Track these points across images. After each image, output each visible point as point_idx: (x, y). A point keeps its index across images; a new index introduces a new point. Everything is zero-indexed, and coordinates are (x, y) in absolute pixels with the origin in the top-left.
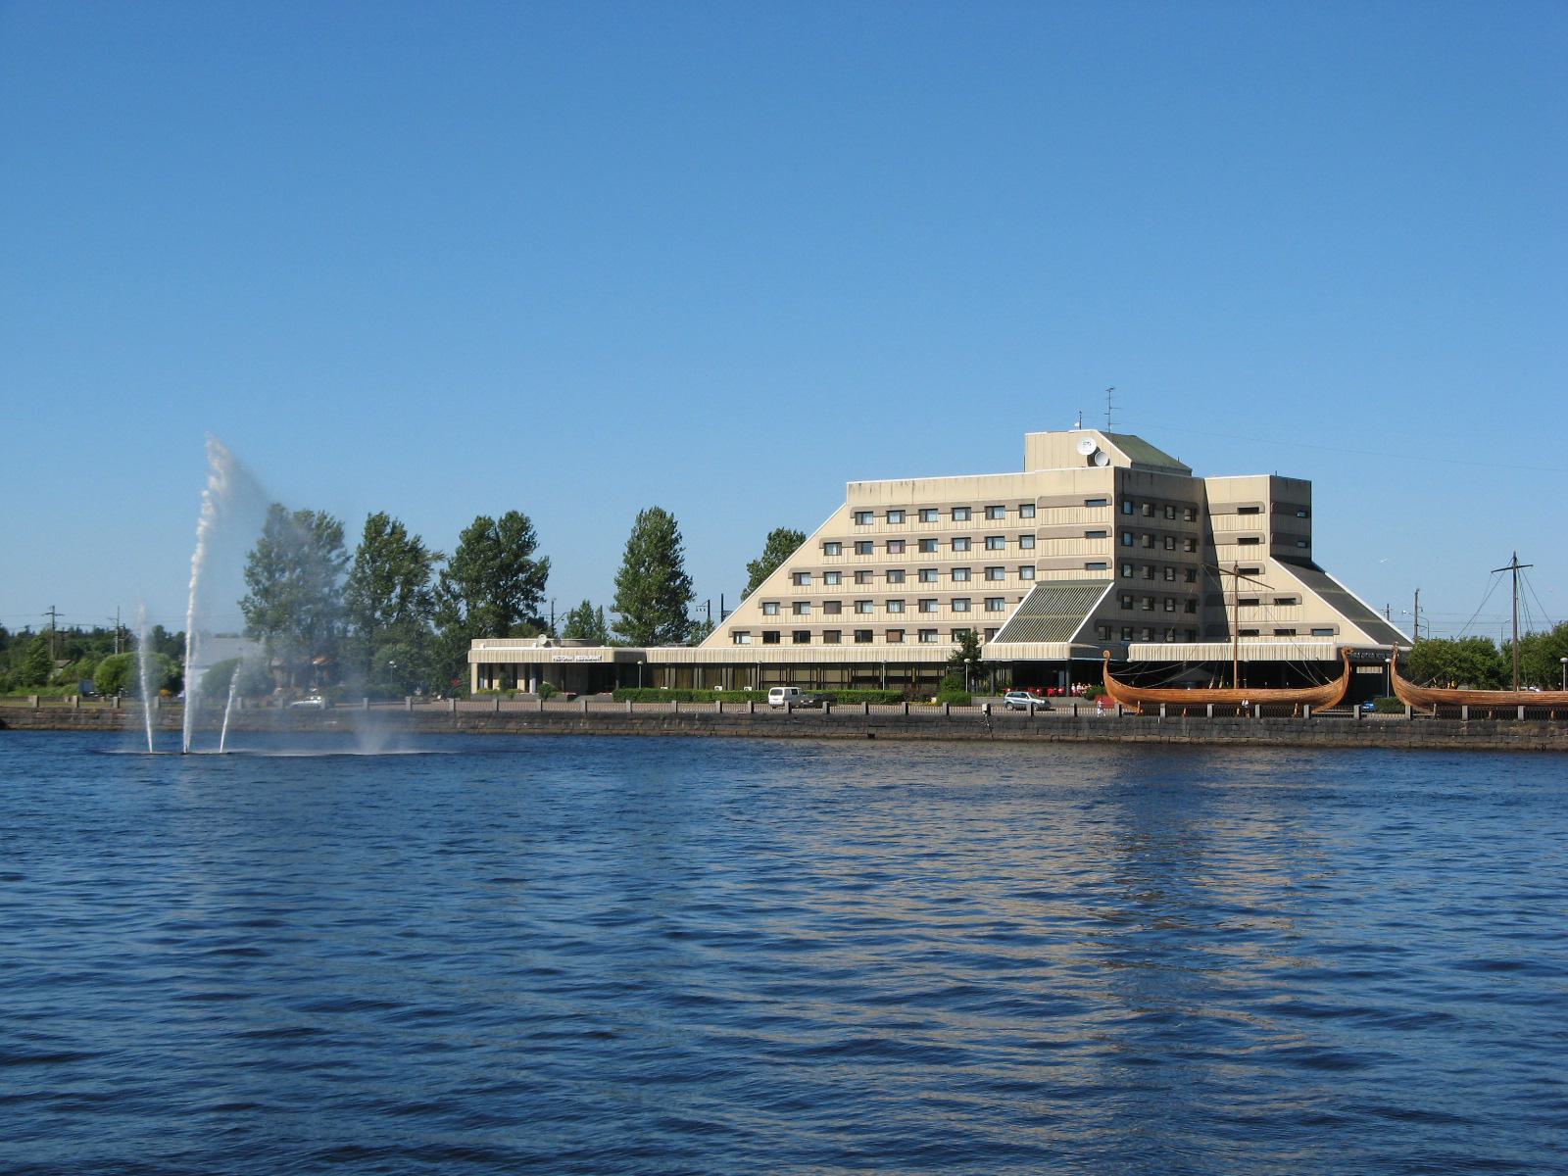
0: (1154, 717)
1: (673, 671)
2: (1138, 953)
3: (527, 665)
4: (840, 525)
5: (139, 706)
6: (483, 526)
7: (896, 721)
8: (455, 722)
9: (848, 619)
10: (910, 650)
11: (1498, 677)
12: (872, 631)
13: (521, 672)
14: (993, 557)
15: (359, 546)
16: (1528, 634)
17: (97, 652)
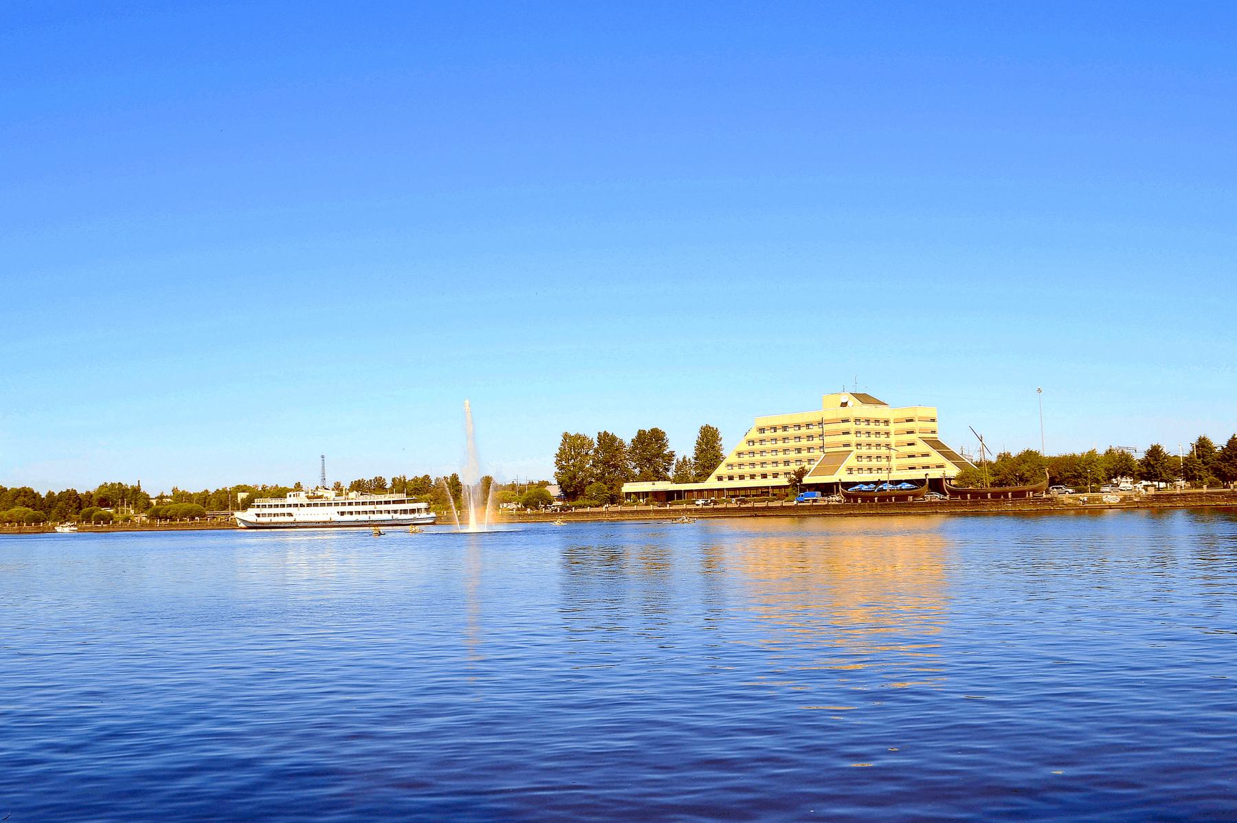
3: (643, 492)
4: (755, 435)
7: (763, 509)
9: (758, 470)
10: (770, 482)
13: (641, 496)
14: (786, 445)
16: (394, 480)
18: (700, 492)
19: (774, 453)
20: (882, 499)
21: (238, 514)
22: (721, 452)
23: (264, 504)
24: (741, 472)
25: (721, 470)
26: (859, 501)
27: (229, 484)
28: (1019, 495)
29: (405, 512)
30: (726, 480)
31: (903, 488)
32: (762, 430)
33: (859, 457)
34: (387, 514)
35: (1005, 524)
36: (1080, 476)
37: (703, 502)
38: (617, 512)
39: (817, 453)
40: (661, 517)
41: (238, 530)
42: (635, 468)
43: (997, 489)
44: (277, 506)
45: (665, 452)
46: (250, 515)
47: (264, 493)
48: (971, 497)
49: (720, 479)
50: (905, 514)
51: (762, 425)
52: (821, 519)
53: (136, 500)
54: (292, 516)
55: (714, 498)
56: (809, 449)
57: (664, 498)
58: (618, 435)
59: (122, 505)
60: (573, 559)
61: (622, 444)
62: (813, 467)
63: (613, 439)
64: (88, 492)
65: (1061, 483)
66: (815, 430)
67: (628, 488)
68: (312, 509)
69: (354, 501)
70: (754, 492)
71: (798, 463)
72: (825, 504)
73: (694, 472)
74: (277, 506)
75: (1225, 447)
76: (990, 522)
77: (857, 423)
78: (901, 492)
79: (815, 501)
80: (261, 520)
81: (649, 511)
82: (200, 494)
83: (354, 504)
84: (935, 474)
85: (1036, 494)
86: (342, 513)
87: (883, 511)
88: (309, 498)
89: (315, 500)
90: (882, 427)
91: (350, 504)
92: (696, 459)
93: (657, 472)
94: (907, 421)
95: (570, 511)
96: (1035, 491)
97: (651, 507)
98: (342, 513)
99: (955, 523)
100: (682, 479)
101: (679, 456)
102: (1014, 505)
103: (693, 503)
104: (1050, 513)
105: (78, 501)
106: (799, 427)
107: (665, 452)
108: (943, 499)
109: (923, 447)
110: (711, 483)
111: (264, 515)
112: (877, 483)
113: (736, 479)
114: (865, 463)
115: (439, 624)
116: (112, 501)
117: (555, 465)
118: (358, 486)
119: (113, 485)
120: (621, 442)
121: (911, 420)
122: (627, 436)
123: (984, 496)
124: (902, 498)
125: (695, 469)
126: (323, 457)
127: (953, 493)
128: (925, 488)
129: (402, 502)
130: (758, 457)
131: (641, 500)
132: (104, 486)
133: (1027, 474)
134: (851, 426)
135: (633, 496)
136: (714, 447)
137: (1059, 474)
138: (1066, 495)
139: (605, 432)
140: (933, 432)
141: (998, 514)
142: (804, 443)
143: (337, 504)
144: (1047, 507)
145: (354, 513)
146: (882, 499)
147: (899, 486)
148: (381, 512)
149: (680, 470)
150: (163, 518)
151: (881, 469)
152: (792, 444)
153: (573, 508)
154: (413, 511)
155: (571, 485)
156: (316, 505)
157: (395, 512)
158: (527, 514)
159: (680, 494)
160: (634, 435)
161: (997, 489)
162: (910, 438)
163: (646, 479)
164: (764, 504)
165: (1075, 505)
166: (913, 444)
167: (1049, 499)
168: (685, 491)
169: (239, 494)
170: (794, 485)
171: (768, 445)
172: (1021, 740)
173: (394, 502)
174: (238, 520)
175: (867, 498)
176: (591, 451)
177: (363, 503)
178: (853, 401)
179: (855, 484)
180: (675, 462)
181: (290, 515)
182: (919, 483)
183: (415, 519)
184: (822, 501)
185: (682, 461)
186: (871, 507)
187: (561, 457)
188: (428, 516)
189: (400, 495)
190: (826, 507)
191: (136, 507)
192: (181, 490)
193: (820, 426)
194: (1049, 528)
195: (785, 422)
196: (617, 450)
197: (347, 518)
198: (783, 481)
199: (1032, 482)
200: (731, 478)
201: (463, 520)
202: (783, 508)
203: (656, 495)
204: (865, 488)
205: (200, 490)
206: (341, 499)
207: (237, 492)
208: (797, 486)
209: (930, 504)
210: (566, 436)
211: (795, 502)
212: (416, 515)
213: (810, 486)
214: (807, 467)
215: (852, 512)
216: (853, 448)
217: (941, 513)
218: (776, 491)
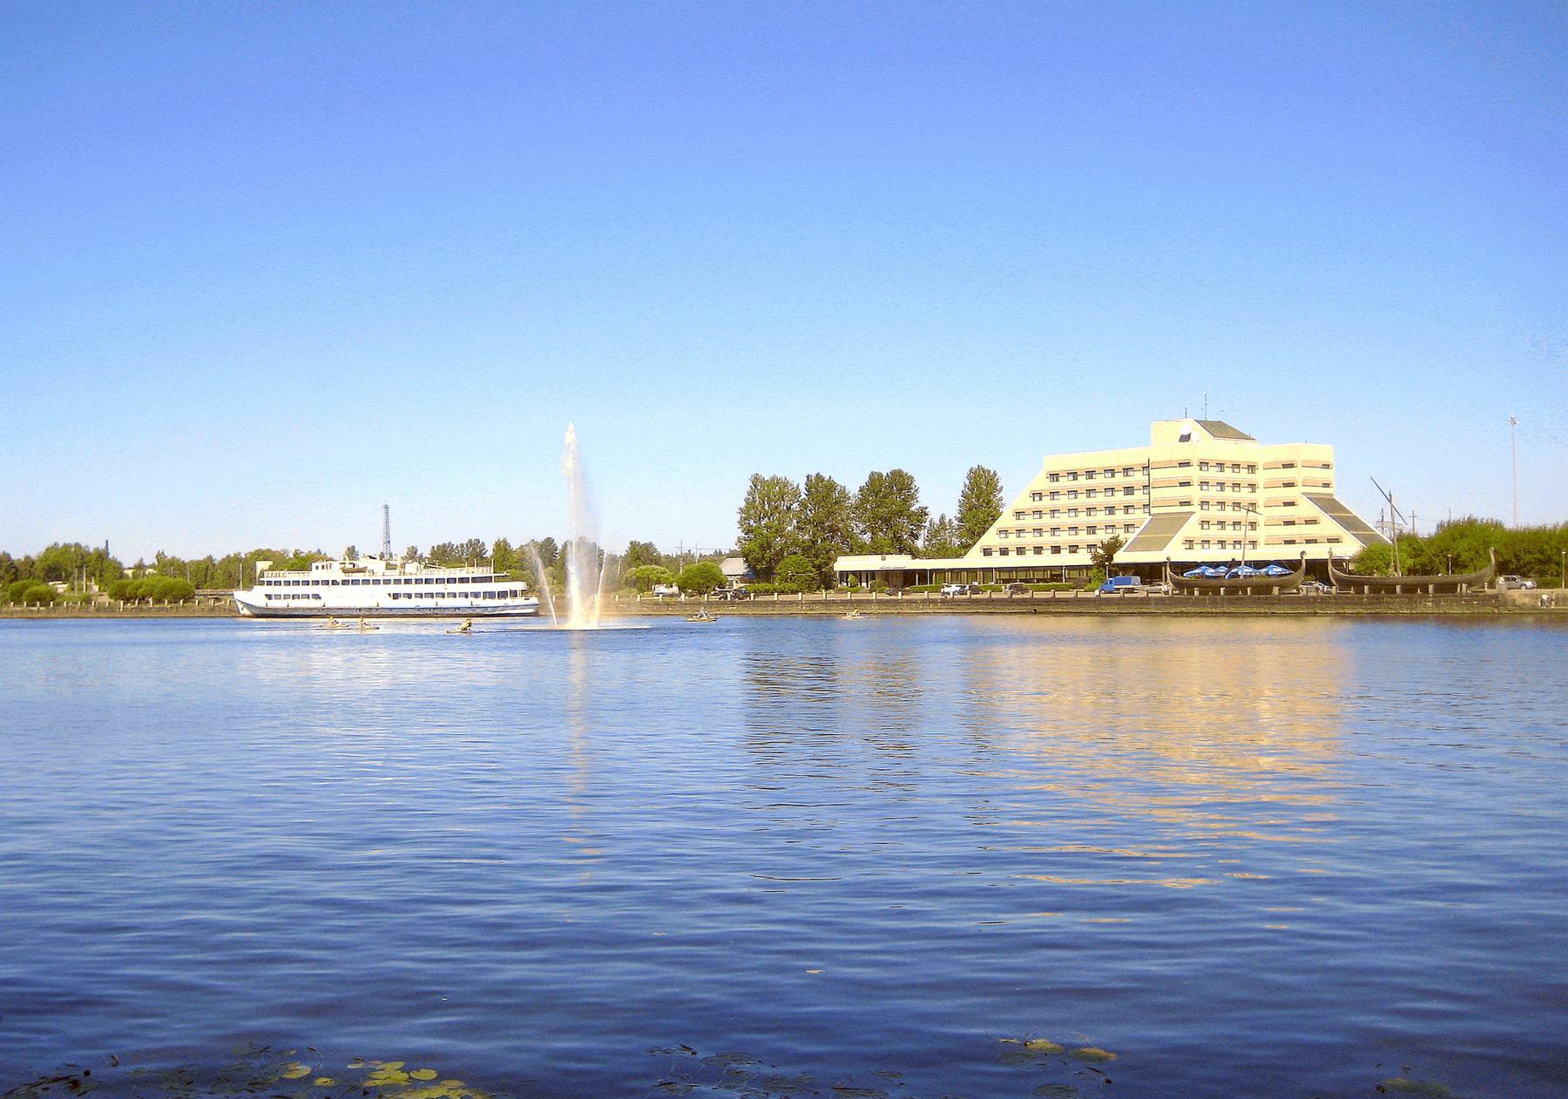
4: (1046, 485)
7: (1047, 601)
9: (1047, 540)
10: (1065, 559)
13: (864, 579)
18: (956, 572)
19: (1072, 514)
20: (1231, 590)
21: (240, 595)
22: (1001, 510)
23: (277, 579)
24: (1021, 542)
25: (990, 538)
26: (1196, 593)
27: (244, 549)
28: (1447, 589)
29: (491, 595)
30: (996, 554)
31: (1270, 573)
32: (1054, 477)
33: (1204, 523)
34: (430, 599)
35: (1429, 631)
36: (1548, 561)
37: (958, 589)
38: (820, 602)
39: (1139, 516)
40: (889, 611)
41: (241, 619)
42: (864, 532)
43: (1413, 579)
44: (297, 583)
45: (913, 509)
46: (256, 597)
47: (280, 561)
48: (1371, 591)
50: (1266, 615)
51: (1055, 469)
52: (1146, 619)
53: (102, 570)
54: (320, 598)
55: (976, 584)
56: (1127, 508)
57: (899, 582)
58: (840, 481)
59: (80, 577)
60: (765, 679)
62: (1131, 537)
63: (831, 486)
64: (27, 558)
65: (1516, 571)
66: (1138, 478)
67: (843, 564)
68: (350, 587)
69: (413, 577)
70: (1039, 575)
71: (1110, 531)
72: (1118, 596)
73: (957, 542)
74: (297, 583)
75: (959, 516)
76: (1398, 629)
77: (1203, 468)
78: (1268, 579)
79: (1131, 591)
80: (274, 604)
81: (869, 602)
82: (198, 563)
83: (413, 582)
84: (1317, 552)
85: (1475, 589)
86: (396, 596)
87: (1232, 610)
88: (345, 571)
89: (354, 574)
90: (1243, 476)
91: (407, 582)
92: (961, 520)
93: (899, 539)
94: (1285, 466)
95: (748, 599)
96: (1470, 585)
97: (873, 596)
98: (396, 596)
99: (1345, 628)
100: (942, 551)
101: (934, 516)
102: (1437, 604)
103: (938, 591)
104: (1494, 619)
105: (13, 570)
106: (1112, 472)
107: (913, 509)
108: (1328, 592)
109: (1307, 509)
110: (974, 559)
111: (278, 597)
112: (1234, 564)
113: (1013, 554)
114: (1214, 532)
116: (66, 571)
117: (738, 525)
118: (443, 556)
119: (67, 546)
120: (843, 490)
121: (1291, 466)
122: (852, 482)
123: (1390, 589)
124: (1263, 589)
125: (961, 536)
126: (386, 507)
127: (1344, 584)
128: (1299, 575)
129: (487, 579)
130: (1047, 520)
131: (864, 584)
132: (55, 547)
133: (1465, 556)
134: (1193, 473)
135: (851, 577)
136: (990, 501)
137: (1516, 556)
138: (1524, 591)
139: (818, 475)
140: (1326, 485)
141: (1412, 618)
142: (1120, 498)
143: (387, 582)
144: (1488, 609)
145: (413, 596)
146: (1231, 590)
147: (1263, 570)
148: (454, 595)
149: (935, 536)
150: (131, 598)
151: (1240, 543)
152: (1100, 499)
153: (752, 595)
154: (503, 595)
155: (763, 558)
156: (355, 582)
157: (476, 595)
158: (680, 603)
159: (924, 576)
160: (863, 480)
161: (1413, 579)
162: (1288, 494)
163: (875, 550)
164: (1048, 595)
165: (1534, 607)
166: (1292, 504)
167: (1495, 597)
168: (932, 571)
169: (258, 563)
170: (1101, 565)
171: (1064, 501)
173: (475, 580)
174: (239, 604)
175: (1209, 588)
176: (796, 504)
177: (427, 581)
178: (1199, 433)
179: (1196, 565)
180: (927, 524)
181: (317, 597)
182: (1292, 565)
183: (506, 607)
184: (1142, 591)
185: (938, 522)
186: (1214, 603)
187: (750, 513)
188: (527, 602)
189: (485, 569)
190: (1145, 601)
191: (100, 582)
192: (169, 555)
193: (1145, 472)
194: (1498, 642)
195: (1090, 466)
196: (836, 503)
197: (403, 603)
198: (1084, 558)
199: (1472, 568)
200: (1004, 552)
201: (562, 608)
202: (1078, 601)
203: (887, 575)
204: (1210, 572)
205: (200, 556)
206: (394, 575)
207: (257, 560)
208: (1104, 567)
209: (1306, 601)
210: (756, 480)
211: (1097, 592)
212: (509, 601)
213: (1126, 568)
214: (1122, 535)
215: (1184, 610)
216: (1195, 508)
217: (1326, 615)
218: (1074, 574)
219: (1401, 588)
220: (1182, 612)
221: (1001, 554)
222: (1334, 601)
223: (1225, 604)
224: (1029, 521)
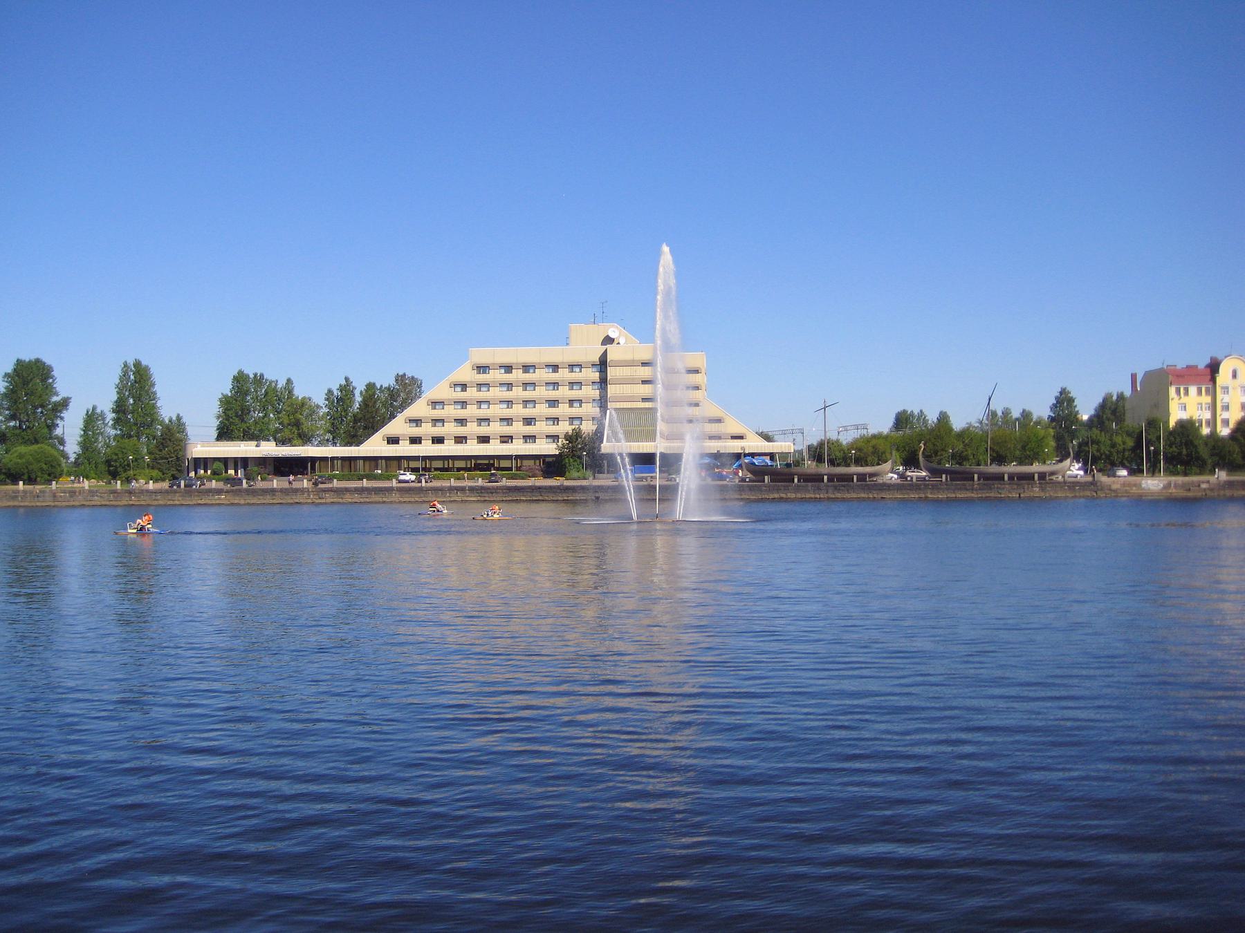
0: (790, 484)
1: (339, 462)
2: (157, 848)
4: (465, 373)
5: (641, 479)
6: (905, 412)
8: (309, 495)
11: (846, 461)
12: (489, 437)
13: (231, 464)
15: (330, 392)
17: (164, 451)
32: (482, 369)
49: (393, 440)
57: (271, 468)
61: (248, 376)
70: (439, 464)
102: (1043, 489)
115: (407, 791)
172: (491, 662)
195: (529, 360)
198: (550, 449)
215: (784, 496)
219: (1039, 477)
220: (781, 498)
221: (433, 443)
222: (945, 486)
223: (830, 491)
224: (451, 411)
